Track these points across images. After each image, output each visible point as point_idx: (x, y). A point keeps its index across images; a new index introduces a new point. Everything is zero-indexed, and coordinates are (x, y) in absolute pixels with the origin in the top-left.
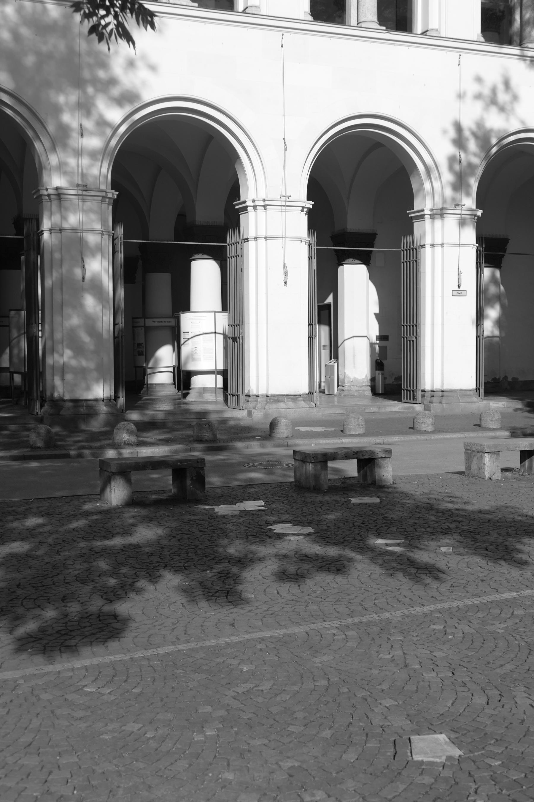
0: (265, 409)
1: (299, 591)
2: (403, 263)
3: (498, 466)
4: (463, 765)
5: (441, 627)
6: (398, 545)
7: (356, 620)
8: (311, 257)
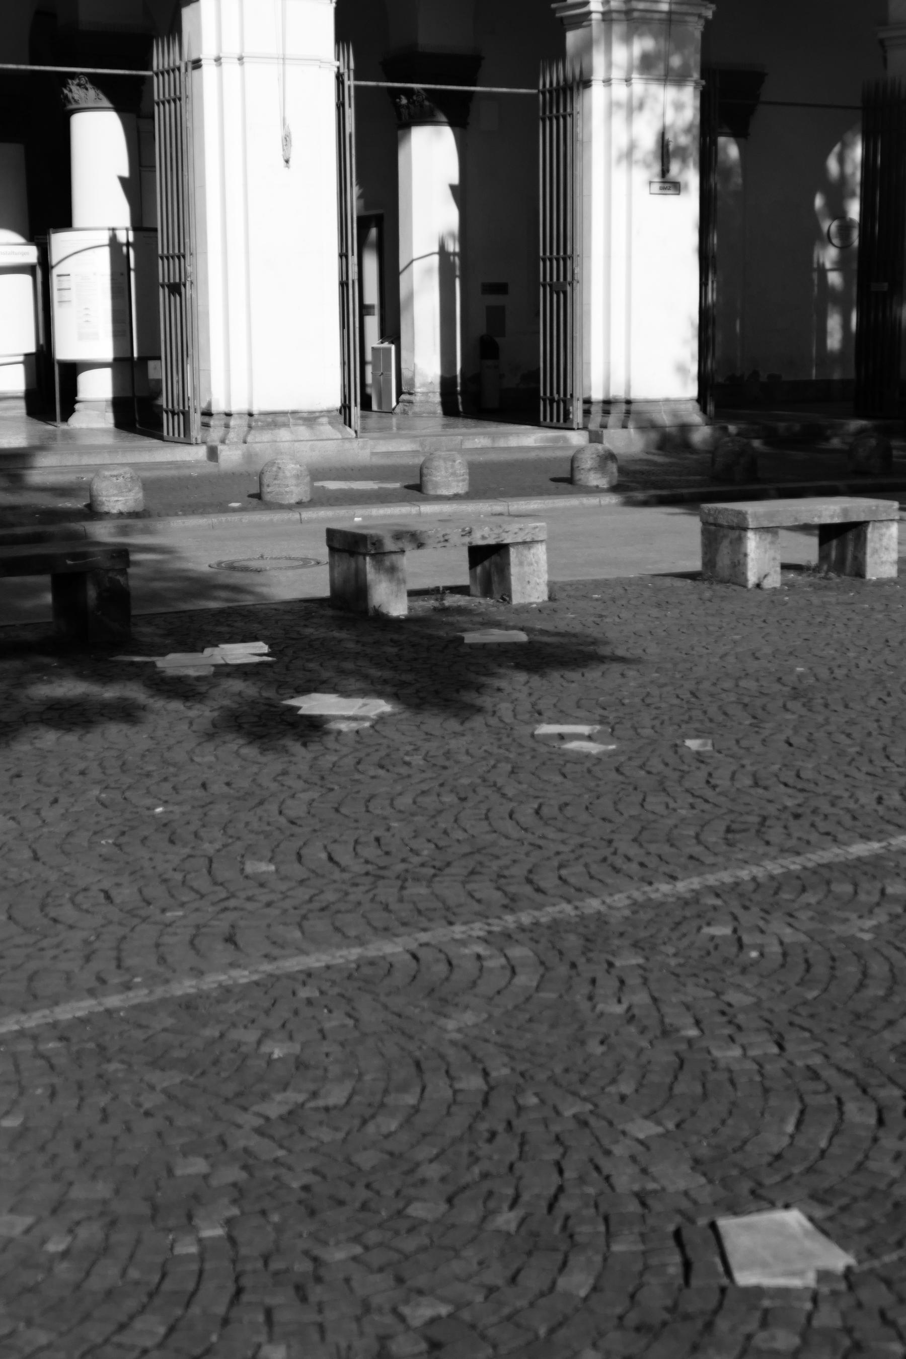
0: (245, 442)
1: (379, 852)
3: (774, 559)
4: (864, 1294)
5: (727, 931)
6: (590, 738)
7: (526, 918)
8: (343, 105)
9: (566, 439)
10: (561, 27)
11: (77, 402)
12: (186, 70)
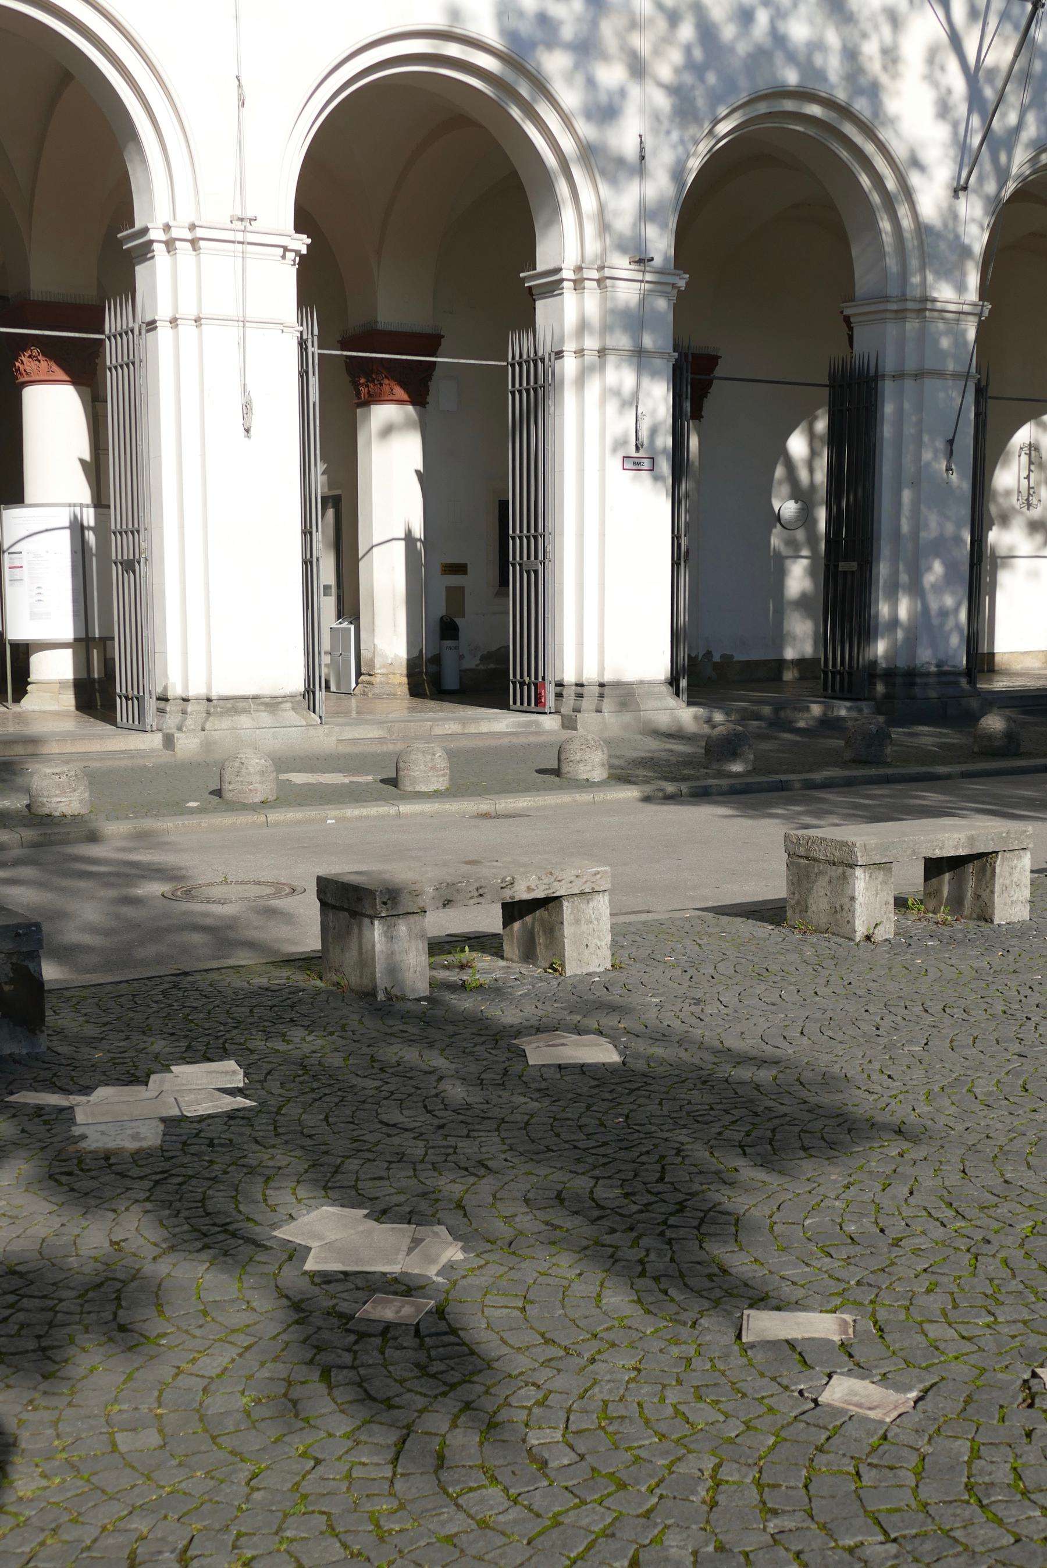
2: (513, 393)
8: (307, 373)
9: (537, 724)
10: (531, 296)
11: (29, 683)
12: (140, 334)
